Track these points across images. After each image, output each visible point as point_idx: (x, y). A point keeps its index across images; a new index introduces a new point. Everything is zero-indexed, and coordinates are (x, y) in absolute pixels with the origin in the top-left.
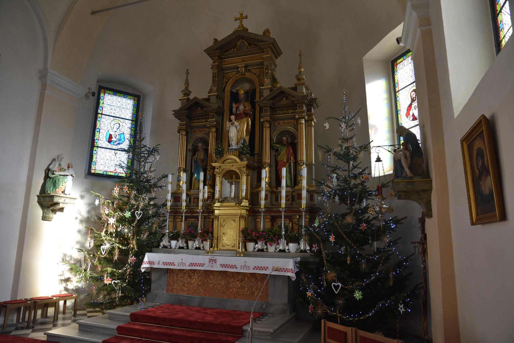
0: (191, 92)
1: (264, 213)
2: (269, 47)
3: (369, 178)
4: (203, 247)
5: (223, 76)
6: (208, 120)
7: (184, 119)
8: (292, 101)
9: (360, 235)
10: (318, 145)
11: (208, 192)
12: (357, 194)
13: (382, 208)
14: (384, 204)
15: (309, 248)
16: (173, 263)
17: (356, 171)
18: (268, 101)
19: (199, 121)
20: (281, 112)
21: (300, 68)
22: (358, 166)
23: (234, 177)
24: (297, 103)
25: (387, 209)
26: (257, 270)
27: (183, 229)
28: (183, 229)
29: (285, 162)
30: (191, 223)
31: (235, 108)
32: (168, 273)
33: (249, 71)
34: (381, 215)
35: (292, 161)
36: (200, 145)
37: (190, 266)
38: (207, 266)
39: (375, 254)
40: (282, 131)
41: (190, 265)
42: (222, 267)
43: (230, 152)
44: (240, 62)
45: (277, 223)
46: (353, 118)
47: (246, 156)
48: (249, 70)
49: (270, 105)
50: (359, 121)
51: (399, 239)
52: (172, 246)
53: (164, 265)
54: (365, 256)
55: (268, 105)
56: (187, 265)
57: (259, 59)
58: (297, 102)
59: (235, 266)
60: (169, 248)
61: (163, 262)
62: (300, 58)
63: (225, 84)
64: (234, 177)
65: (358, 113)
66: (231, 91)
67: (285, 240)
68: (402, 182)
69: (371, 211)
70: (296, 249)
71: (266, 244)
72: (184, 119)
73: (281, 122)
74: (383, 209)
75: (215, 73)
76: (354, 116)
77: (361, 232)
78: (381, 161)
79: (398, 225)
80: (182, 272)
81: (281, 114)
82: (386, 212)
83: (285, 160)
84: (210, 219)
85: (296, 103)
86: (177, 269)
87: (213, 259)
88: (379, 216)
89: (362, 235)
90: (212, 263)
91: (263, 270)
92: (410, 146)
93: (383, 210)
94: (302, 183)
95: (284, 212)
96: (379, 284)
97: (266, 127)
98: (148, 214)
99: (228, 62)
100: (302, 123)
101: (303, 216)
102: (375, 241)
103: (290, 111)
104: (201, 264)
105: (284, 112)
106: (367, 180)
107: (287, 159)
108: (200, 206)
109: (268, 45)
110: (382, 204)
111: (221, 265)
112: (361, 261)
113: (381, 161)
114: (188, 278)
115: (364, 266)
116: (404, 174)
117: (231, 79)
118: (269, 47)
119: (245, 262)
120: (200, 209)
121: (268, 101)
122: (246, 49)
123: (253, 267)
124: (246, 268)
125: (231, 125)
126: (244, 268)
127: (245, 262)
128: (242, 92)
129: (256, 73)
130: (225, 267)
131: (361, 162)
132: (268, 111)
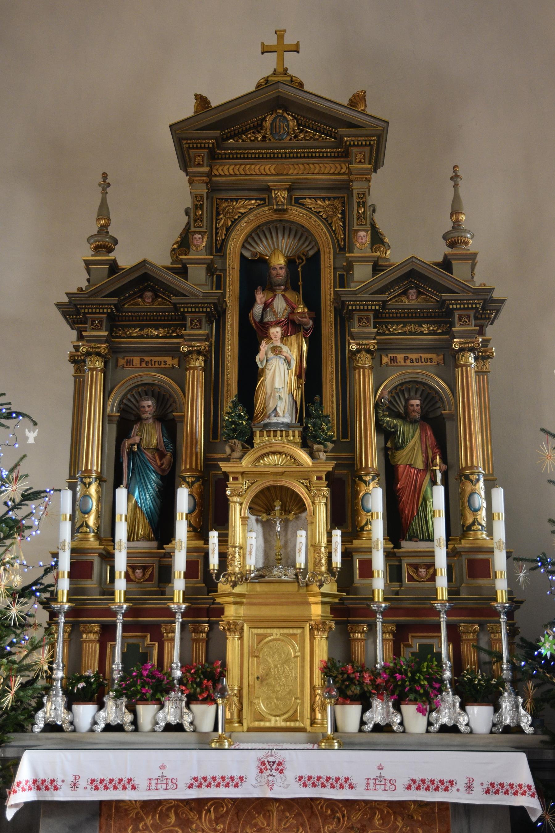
0: (116, 242)
1: (382, 616)
2: (368, 143)
4: (401, 724)
5: (217, 208)
6: (184, 333)
7: (101, 322)
8: (174, 304)
10: (544, 427)
11: (189, 551)
16: (130, 780)
18: (371, 294)
19: (143, 332)
20: (400, 329)
21: (459, 213)
23: (278, 508)
24: (188, 312)
26: (418, 792)
27: (118, 665)
28: (118, 665)
29: (419, 470)
30: (128, 645)
31: (262, 306)
32: (100, 815)
33: (298, 202)
35: (438, 468)
36: (149, 406)
37: (191, 786)
38: (253, 785)
40: (411, 379)
41: (192, 784)
42: (305, 785)
43: (275, 432)
44: (272, 174)
45: (410, 646)
47: (325, 447)
48: (297, 200)
49: (208, 310)
52: (77, 721)
53: (97, 788)
55: (468, 304)
56: (182, 784)
57: (328, 174)
58: (456, 304)
59: (347, 779)
60: (70, 732)
61: (93, 781)
62: (456, 186)
63: (225, 232)
64: (278, 508)
66: (242, 256)
67: (457, 697)
70: (491, 724)
71: (397, 708)
72: (101, 322)
73: (400, 357)
75: (202, 197)
80: (155, 809)
81: (399, 334)
83: (420, 464)
84: (202, 632)
85: (186, 310)
86: (136, 801)
87: (271, 759)
90: (271, 775)
91: (437, 789)
94: (371, 530)
95: (448, 613)
97: (363, 367)
98: (6, 619)
99: (233, 169)
100: (467, 365)
101: (379, 626)
103: (428, 328)
104: (232, 778)
105: (407, 329)
107: (423, 462)
108: (179, 592)
109: (355, 137)
111: (300, 780)
114: (177, 829)
117: (246, 219)
118: (368, 143)
119: (380, 768)
120: (120, 602)
121: (371, 294)
122: (291, 139)
123: (407, 783)
124: (383, 787)
125: (271, 355)
126: (377, 787)
127: (380, 768)
128: (279, 261)
129: (320, 212)
130: (314, 785)
132: (368, 322)
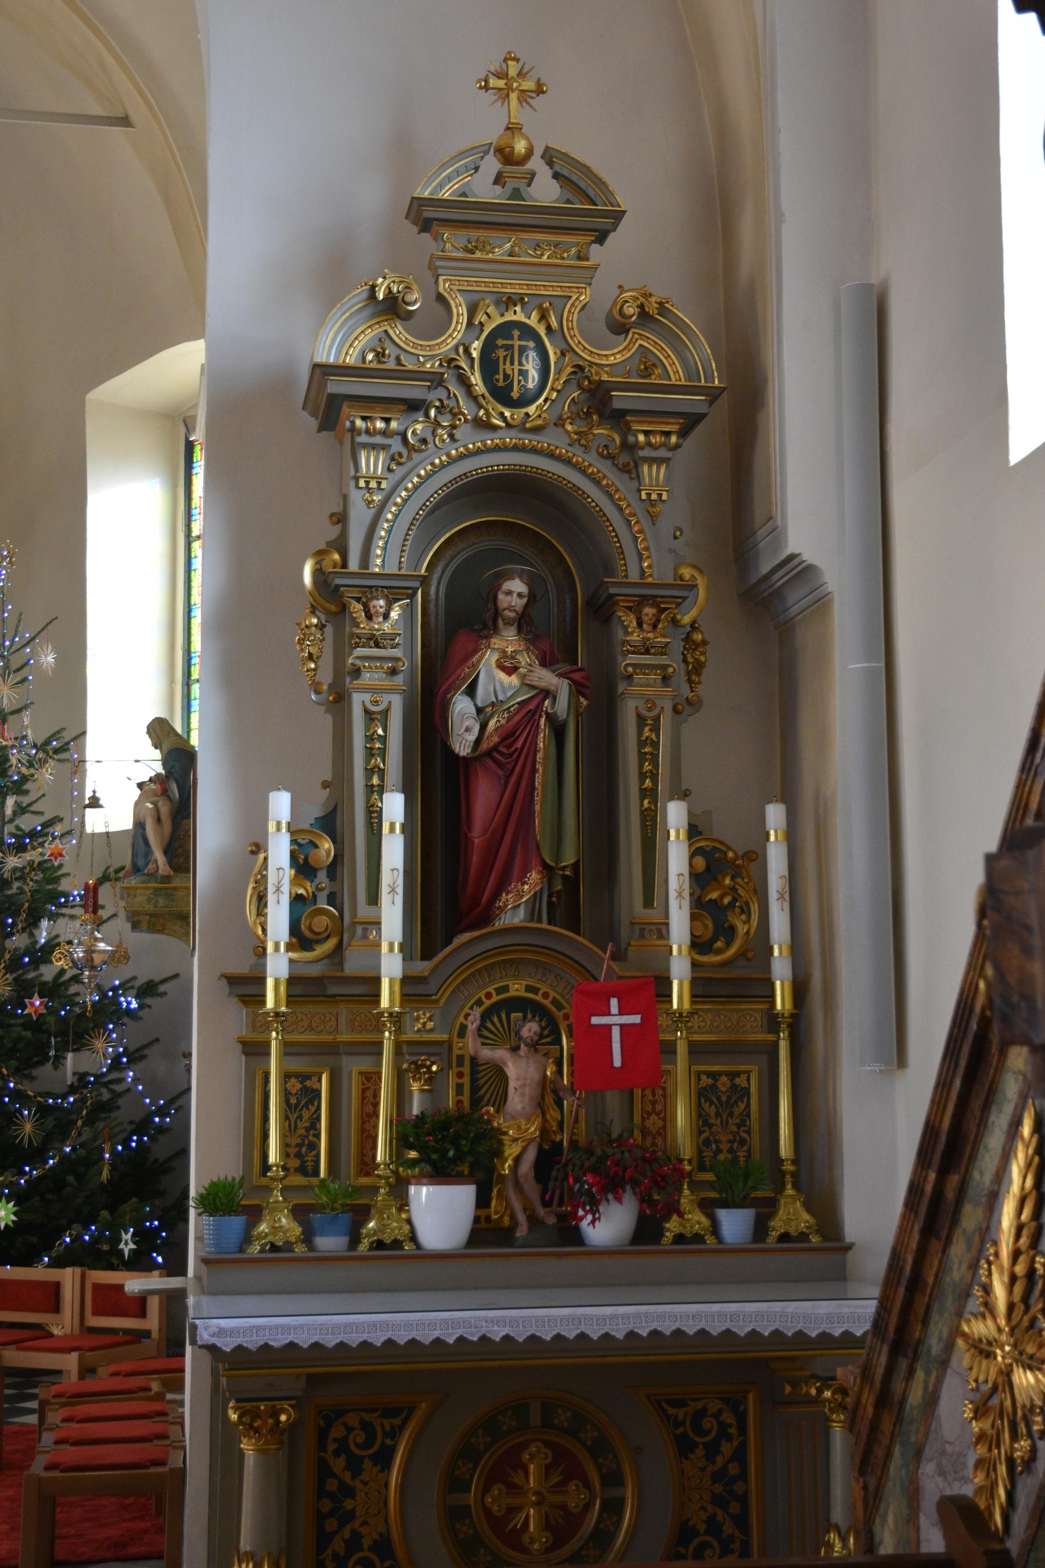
3: (64, 853)
9: (24, 1033)
12: (23, 905)
13: (93, 951)
14: (102, 940)
15: (710, 924)
17: (27, 823)
22: (33, 808)
25: (108, 955)
34: (90, 971)
39: (72, 1090)
46: (25, 646)
50: (49, 659)
51: (150, 1044)
54: (35, 1097)
65: (46, 630)
68: (141, 888)
69: (60, 959)
74: (94, 955)
76: (33, 639)
77: (28, 1024)
78: (100, 806)
79: (149, 1001)
82: (105, 963)
88: (82, 974)
89: (28, 1034)
92: (174, 787)
93: (97, 959)
96: (71, 1179)
102: (68, 1051)
106: (56, 859)
110: (96, 939)
112: (22, 1115)
113: (100, 806)
115: (28, 1128)
116: (151, 867)
131: (43, 795)
